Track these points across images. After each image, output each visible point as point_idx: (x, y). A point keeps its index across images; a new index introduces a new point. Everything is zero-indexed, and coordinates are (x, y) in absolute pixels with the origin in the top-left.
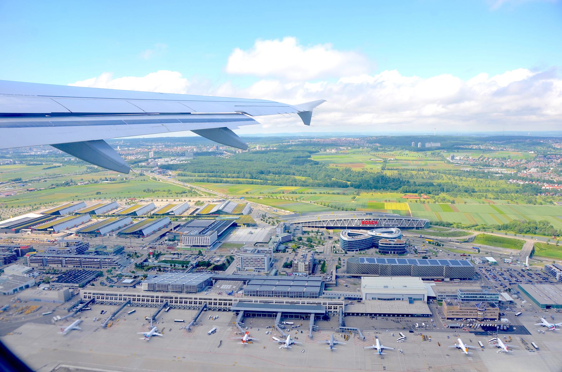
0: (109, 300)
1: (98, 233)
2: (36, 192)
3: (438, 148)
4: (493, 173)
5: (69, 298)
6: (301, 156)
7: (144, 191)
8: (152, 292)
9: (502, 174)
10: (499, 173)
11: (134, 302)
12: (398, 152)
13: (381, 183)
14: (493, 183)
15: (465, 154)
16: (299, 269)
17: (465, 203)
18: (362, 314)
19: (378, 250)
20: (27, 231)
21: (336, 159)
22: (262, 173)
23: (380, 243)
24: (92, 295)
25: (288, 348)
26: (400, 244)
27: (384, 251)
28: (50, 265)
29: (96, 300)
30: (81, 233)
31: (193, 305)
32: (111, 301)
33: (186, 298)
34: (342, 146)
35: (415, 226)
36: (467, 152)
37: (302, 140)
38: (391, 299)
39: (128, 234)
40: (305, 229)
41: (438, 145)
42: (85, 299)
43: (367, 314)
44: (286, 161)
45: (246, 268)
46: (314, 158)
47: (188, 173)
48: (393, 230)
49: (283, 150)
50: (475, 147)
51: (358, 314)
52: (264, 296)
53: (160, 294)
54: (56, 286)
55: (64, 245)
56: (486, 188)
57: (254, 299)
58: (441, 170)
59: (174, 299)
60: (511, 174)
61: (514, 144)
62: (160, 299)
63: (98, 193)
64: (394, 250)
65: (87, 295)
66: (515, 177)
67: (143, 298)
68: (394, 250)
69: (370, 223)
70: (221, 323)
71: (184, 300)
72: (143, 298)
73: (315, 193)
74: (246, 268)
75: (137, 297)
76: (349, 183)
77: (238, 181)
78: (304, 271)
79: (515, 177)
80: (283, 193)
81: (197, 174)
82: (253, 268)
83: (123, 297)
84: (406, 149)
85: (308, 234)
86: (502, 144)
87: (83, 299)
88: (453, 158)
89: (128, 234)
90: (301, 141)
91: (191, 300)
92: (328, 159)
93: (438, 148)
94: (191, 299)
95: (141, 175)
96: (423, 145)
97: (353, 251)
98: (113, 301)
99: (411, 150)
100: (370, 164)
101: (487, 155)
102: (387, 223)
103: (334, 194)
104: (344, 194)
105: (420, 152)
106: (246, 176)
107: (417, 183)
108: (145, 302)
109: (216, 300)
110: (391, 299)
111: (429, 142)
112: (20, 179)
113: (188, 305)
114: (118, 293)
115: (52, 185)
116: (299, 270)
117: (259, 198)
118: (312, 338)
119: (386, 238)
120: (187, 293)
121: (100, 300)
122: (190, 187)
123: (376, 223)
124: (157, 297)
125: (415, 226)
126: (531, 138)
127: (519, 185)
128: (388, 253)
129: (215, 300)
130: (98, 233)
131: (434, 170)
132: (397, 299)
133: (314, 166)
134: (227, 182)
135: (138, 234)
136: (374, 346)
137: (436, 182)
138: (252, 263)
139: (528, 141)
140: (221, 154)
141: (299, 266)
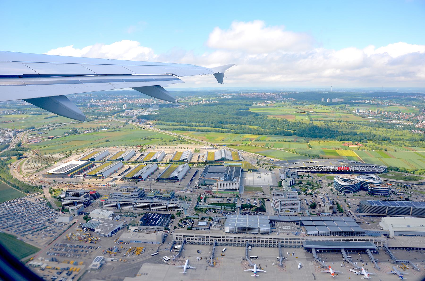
0: (198, 241)
1: (140, 178)
2: (55, 139)
3: (343, 103)
4: (396, 124)
5: (164, 239)
6: (242, 108)
7: (142, 139)
8: (232, 234)
9: (403, 125)
10: (400, 125)
11: (219, 242)
12: (314, 105)
13: (313, 133)
14: (400, 132)
15: (365, 108)
16: (325, 210)
17: (395, 150)
18: (399, 248)
19: (367, 192)
20: (79, 177)
21: (270, 110)
22: (221, 122)
23: (370, 187)
24: (182, 237)
25: (184, 274)
26: (386, 188)
27: (374, 193)
28: (123, 208)
29: (187, 241)
30: (126, 178)
31: (269, 243)
32: (200, 241)
33: (295, 239)
34: (268, 100)
35: (377, 171)
36: (365, 106)
37: (232, 94)
38: (413, 236)
39: (165, 179)
40: (300, 174)
41: (342, 100)
42: (177, 240)
43: (403, 248)
44: (232, 113)
45: (284, 210)
46: (251, 110)
47: (164, 123)
48: (373, 176)
49: (223, 102)
50: (367, 102)
51: (396, 248)
52: (323, 235)
53: (241, 236)
54: (143, 228)
55: (124, 190)
56: (398, 137)
57: (317, 238)
58: (355, 122)
59: (206, 238)
60: (409, 125)
61: (394, 100)
62: (241, 239)
63: (107, 141)
64: (381, 192)
65: (179, 237)
66: (410, 128)
67: (227, 239)
68: (381, 192)
69: (344, 169)
70: (298, 259)
71: (261, 240)
72: (227, 239)
73: (275, 141)
74: (284, 210)
75: (221, 238)
76: (292, 132)
77: (207, 130)
78: (329, 211)
79: (410, 128)
80: (251, 141)
81: (171, 124)
82: (289, 210)
83: (210, 238)
84: (318, 103)
85: (302, 178)
86: (385, 99)
87: (175, 240)
88: (358, 111)
89: (165, 179)
90: (232, 96)
91: (267, 240)
92: (264, 111)
93: (343, 103)
94: (267, 239)
95: (127, 124)
96: (331, 100)
97: (349, 193)
98: (202, 241)
99: (322, 104)
100: (299, 116)
101: (381, 109)
102: (356, 169)
103: (289, 141)
104: (297, 142)
105: (330, 106)
106: (210, 126)
107: (344, 133)
108: (229, 242)
109: (271, 239)
110: (413, 236)
111: (335, 98)
112: (34, 128)
113: (265, 243)
114: (206, 235)
115: (65, 133)
116: (325, 211)
117: (237, 145)
118: (282, 266)
119: (373, 183)
120: (262, 234)
121: (190, 241)
122: (178, 136)
123: (348, 169)
124: (239, 238)
125: (377, 171)
126: (406, 94)
127: (420, 135)
128: (377, 195)
129: (287, 239)
130: (140, 178)
131: (350, 122)
132: (418, 235)
133: (257, 117)
134: (199, 131)
135: (138, 178)
136: (252, 270)
137: (358, 132)
138: (288, 206)
139: (403, 97)
140: (177, 106)
141: (325, 207)
